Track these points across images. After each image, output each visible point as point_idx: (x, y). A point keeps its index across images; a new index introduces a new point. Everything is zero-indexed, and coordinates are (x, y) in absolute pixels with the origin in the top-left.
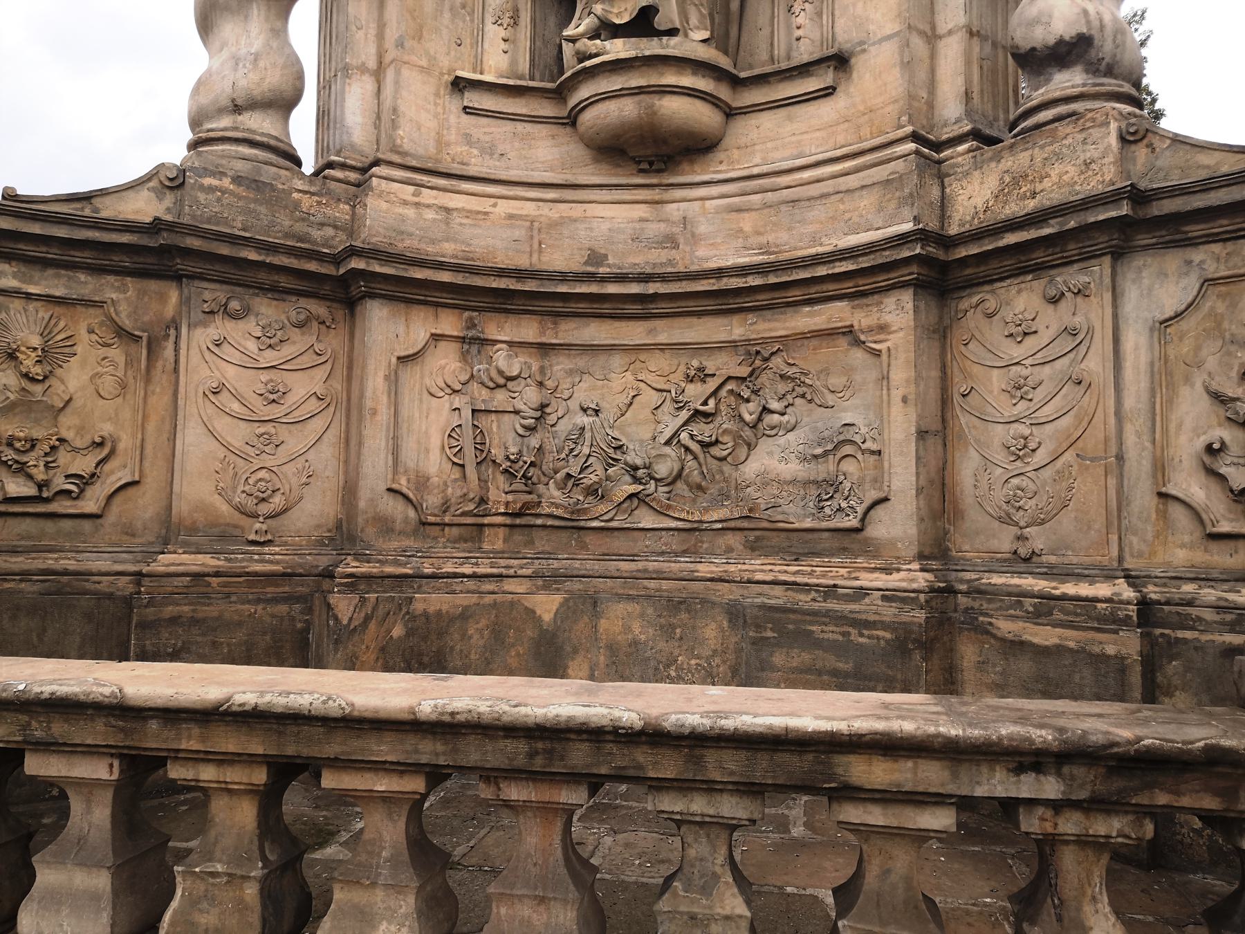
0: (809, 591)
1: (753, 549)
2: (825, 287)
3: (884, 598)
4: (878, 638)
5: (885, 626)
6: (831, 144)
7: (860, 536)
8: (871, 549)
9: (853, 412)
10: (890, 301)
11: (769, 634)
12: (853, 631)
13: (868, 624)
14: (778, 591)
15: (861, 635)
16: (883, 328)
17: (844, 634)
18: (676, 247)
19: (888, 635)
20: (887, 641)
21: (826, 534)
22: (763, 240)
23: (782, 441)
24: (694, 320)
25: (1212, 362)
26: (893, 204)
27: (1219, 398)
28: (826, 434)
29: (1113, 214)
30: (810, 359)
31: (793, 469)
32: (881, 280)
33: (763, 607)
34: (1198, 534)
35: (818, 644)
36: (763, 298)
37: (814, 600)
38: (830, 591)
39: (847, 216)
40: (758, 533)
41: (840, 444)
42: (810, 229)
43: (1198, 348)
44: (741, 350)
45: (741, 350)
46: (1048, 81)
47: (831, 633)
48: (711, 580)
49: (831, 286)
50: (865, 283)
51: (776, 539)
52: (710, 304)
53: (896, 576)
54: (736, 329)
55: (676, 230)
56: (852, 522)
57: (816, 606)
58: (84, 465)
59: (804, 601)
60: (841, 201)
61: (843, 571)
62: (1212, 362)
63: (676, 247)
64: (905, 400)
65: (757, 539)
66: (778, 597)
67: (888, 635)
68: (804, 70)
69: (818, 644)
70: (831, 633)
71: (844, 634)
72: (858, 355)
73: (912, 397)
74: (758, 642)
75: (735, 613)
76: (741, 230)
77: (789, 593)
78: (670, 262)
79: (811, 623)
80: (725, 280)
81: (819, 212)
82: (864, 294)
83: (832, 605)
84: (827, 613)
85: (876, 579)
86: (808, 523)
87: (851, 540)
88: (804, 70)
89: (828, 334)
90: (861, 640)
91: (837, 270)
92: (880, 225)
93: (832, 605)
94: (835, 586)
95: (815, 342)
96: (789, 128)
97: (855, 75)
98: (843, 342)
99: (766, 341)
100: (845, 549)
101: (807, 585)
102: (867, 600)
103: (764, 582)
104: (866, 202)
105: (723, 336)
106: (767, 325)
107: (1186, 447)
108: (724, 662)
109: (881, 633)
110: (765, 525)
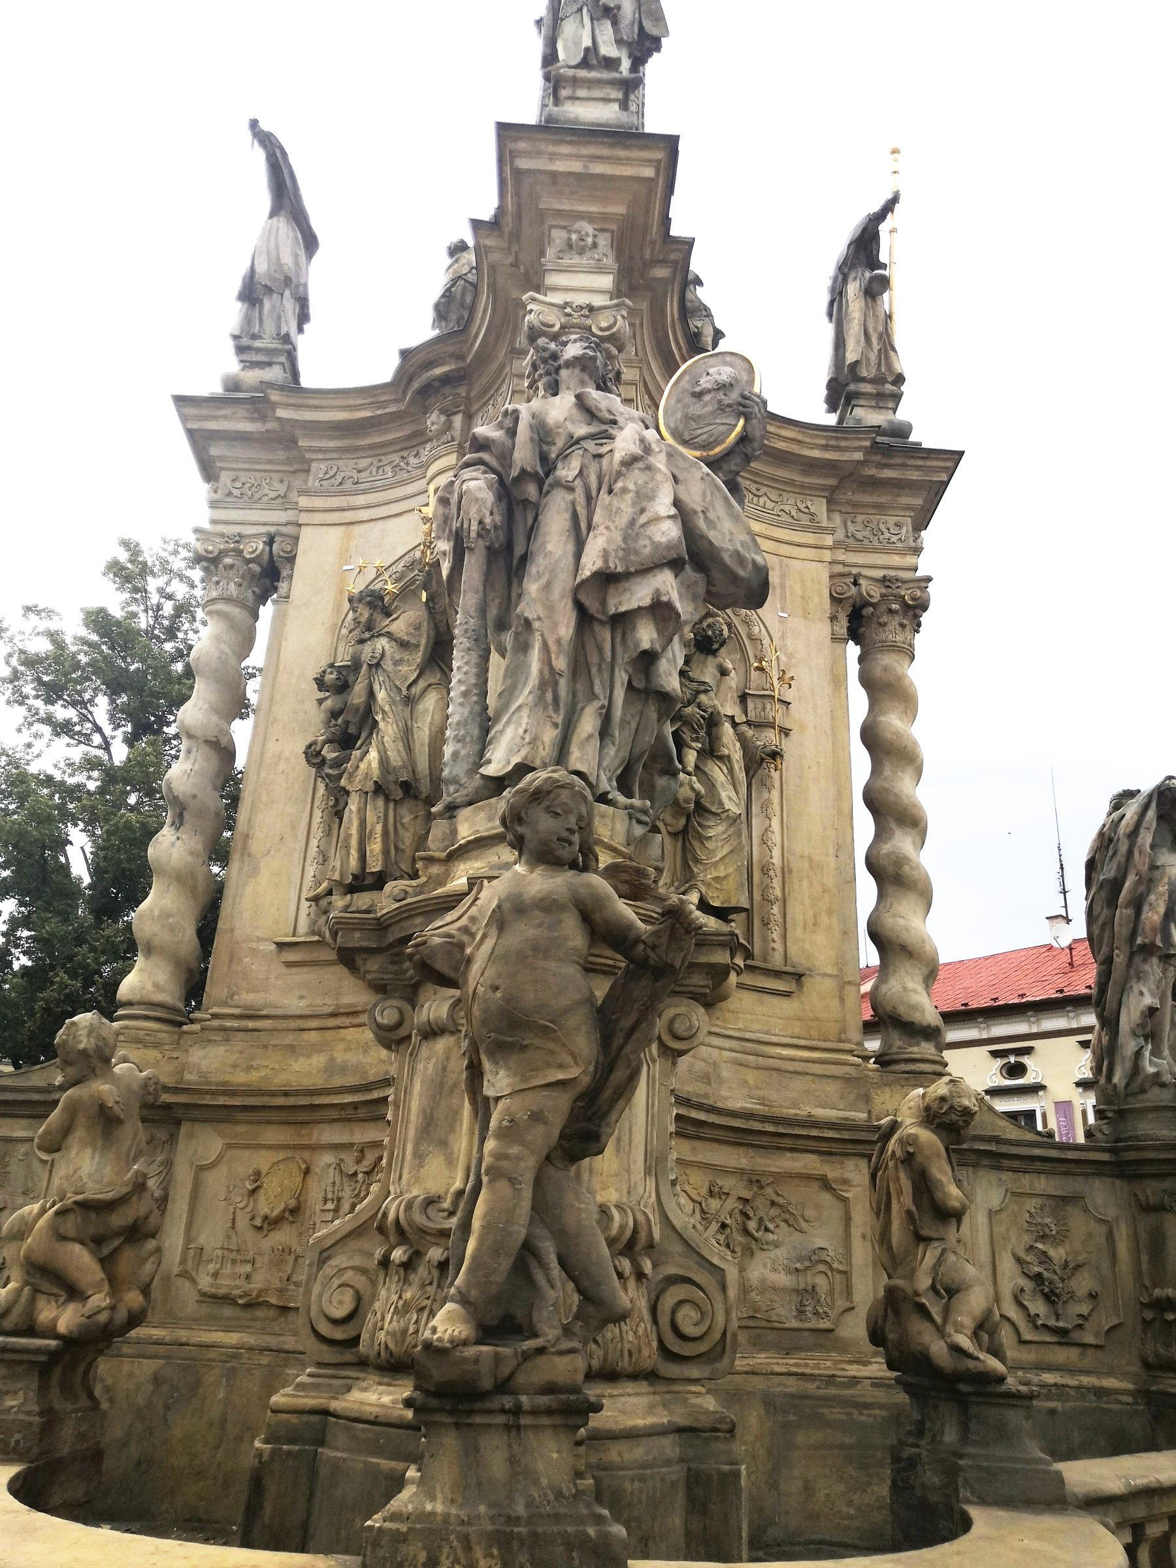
0: (814, 1380)
1: (754, 1344)
2: (799, 1142)
3: (873, 1385)
4: (875, 1416)
5: (881, 1406)
6: (789, 1032)
7: (830, 1335)
8: (841, 1346)
9: (822, 1238)
10: (850, 1164)
11: (792, 1418)
12: (856, 1412)
13: (867, 1406)
14: (791, 1381)
15: (862, 1414)
16: (845, 1182)
17: (848, 1414)
18: (709, 1084)
19: (883, 1413)
20: (884, 1418)
21: (807, 1333)
22: (761, 1093)
23: (772, 1254)
24: (716, 1145)
25: (1013, 1239)
26: (852, 1097)
27: (1019, 1260)
28: (803, 1253)
29: (988, 1148)
30: (792, 1194)
31: (782, 1279)
32: (849, 1148)
33: (786, 1395)
34: (1016, 1339)
35: (830, 1424)
36: (765, 1140)
37: (818, 1388)
38: (830, 1380)
39: (818, 1094)
40: (758, 1331)
41: (813, 1259)
42: (793, 1095)
43: (1008, 1230)
44: (746, 1177)
45: (746, 1177)
46: (918, 1044)
47: (837, 1414)
48: (747, 1373)
49: (812, 1143)
50: (835, 1147)
51: (771, 1336)
52: (732, 1137)
53: (870, 1368)
54: (738, 1158)
55: (711, 1070)
56: (825, 1324)
57: (822, 1392)
58: (1084, 1309)
59: (811, 1387)
60: (813, 1081)
61: (828, 1364)
62: (1013, 1239)
63: (709, 1084)
64: (864, 1236)
65: (759, 1336)
66: (792, 1385)
67: (883, 1413)
68: (778, 974)
69: (830, 1424)
70: (837, 1414)
71: (848, 1414)
72: (826, 1198)
73: (869, 1235)
74: (786, 1426)
75: (769, 1402)
76: (746, 1082)
77: (800, 1382)
78: (706, 1096)
79: (823, 1406)
80: (751, 1122)
81: (798, 1084)
82: (830, 1154)
83: (832, 1391)
84: (834, 1398)
85: (860, 1371)
86: (795, 1324)
87: (825, 1338)
88: (778, 974)
89: (807, 1178)
90: (863, 1418)
91: (825, 1135)
92: (842, 1107)
93: (832, 1391)
94: (833, 1376)
95: (796, 1181)
96: (759, 1009)
97: (805, 990)
98: (815, 1185)
99: (764, 1174)
100: (820, 1345)
101: (812, 1375)
102: (859, 1387)
103: (782, 1374)
104: (831, 1088)
105: (734, 1164)
106: (763, 1161)
107: (1006, 1289)
108: (762, 1445)
109: (877, 1412)
110: (764, 1324)
